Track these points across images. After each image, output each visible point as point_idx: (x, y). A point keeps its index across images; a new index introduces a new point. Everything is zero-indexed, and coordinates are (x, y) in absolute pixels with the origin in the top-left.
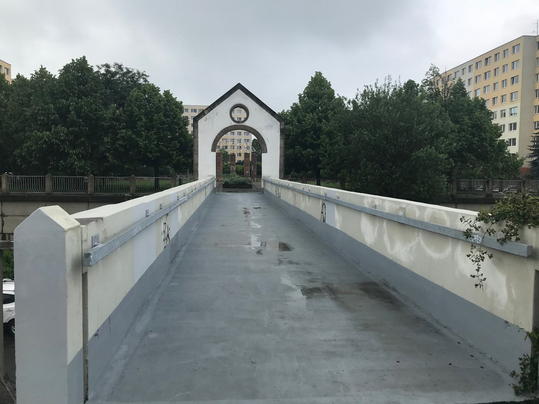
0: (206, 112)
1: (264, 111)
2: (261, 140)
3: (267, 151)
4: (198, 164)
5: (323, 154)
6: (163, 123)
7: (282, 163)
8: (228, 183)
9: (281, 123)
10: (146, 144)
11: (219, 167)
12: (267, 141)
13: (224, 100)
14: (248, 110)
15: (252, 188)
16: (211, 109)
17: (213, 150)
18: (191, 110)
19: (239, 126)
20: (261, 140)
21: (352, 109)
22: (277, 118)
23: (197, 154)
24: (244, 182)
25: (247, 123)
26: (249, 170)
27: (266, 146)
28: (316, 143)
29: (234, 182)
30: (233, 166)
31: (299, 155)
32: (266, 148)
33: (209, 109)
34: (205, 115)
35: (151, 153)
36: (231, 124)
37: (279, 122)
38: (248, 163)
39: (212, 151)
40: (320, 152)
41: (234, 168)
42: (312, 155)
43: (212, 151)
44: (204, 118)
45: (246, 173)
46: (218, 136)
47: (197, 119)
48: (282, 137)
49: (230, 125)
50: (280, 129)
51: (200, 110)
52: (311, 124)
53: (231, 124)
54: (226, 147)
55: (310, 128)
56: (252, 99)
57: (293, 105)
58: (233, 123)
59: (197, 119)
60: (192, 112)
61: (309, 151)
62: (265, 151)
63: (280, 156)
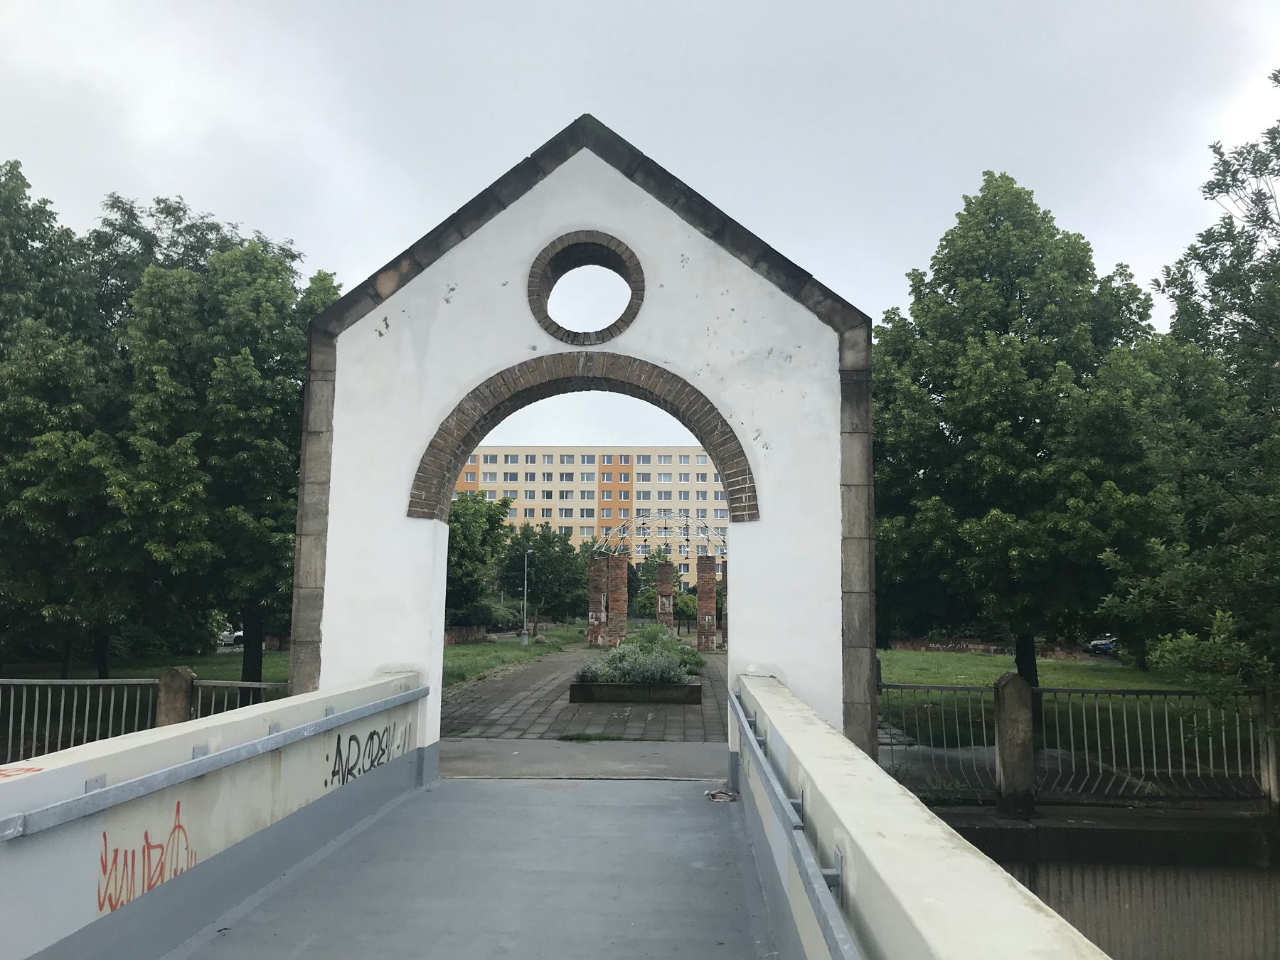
0: (384, 286)
1: (737, 269)
2: (723, 444)
3: (756, 507)
4: (322, 597)
5: (1086, 535)
6: (255, 397)
7: (857, 588)
8: (595, 677)
9: (847, 335)
10: (146, 495)
11: (618, 601)
12: (757, 446)
13: (499, 211)
14: (638, 264)
15: (699, 702)
16: (419, 268)
17: (421, 507)
18: (581, 457)
19: (582, 360)
20: (723, 444)
21: (900, 518)
22: (819, 308)
23: (322, 534)
24: (663, 673)
25: (627, 344)
26: (714, 613)
27: (752, 480)
28: (1030, 481)
29: (625, 674)
30: (664, 599)
31: (938, 543)
32: (753, 489)
33: (405, 266)
34: (378, 299)
35: (170, 539)
36: (534, 348)
37: (829, 328)
38: (711, 590)
39: (410, 514)
40: (1065, 525)
41: (667, 606)
42: (1019, 540)
43: (410, 514)
44: (374, 317)
45: (704, 622)
46: (452, 424)
47: (332, 328)
48: (856, 421)
49: (526, 355)
50: (842, 372)
51: (604, 456)
52: (995, 385)
53: (534, 348)
54: (668, 550)
55: (989, 406)
56: (663, 198)
57: (884, 321)
58: (549, 346)
59: (332, 328)
60: (583, 462)
61: (998, 521)
62: (743, 509)
63: (844, 539)
